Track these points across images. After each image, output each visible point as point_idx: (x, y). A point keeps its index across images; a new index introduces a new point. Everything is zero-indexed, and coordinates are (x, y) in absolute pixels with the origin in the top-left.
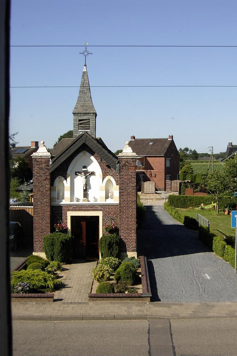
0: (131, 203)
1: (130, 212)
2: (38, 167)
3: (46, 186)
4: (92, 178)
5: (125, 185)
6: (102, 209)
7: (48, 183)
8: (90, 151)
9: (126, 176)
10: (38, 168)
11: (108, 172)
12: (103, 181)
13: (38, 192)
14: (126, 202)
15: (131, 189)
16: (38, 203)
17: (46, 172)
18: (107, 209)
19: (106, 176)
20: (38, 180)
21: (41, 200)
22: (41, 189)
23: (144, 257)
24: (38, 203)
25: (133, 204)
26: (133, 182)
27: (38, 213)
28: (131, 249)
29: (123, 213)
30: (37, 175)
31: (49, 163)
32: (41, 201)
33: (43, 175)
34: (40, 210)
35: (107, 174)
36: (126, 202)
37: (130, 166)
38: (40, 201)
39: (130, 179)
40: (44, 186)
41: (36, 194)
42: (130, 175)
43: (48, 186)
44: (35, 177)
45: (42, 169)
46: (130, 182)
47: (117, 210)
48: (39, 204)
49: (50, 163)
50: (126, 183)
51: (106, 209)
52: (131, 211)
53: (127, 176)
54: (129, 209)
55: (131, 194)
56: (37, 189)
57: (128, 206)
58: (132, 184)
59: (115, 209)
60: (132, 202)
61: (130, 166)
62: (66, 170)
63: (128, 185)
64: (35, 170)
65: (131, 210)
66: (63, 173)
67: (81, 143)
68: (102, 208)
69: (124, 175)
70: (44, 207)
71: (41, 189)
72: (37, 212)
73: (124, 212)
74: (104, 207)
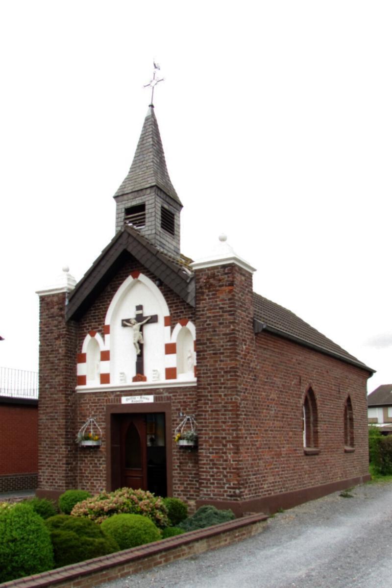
0: (223, 376)
1: (223, 397)
4: (149, 329)
5: (208, 332)
6: (170, 397)
9: (211, 309)
14: (212, 373)
21: (51, 379)
25: (229, 377)
28: (226, 491)
34: (48, 401)
42: (221, 306)
46: (220, 324)
48: (47, 388)
49: (67, 303)
51: (179, 395)
52: (225, 395)
55: (223, 353)
60: (226, 372)
63: (215, 331)
65: (222, 394)
66: (99, 325)
67: (120, 250)
68: (171, 395)
69: (206, 309)
73: (208, 400)
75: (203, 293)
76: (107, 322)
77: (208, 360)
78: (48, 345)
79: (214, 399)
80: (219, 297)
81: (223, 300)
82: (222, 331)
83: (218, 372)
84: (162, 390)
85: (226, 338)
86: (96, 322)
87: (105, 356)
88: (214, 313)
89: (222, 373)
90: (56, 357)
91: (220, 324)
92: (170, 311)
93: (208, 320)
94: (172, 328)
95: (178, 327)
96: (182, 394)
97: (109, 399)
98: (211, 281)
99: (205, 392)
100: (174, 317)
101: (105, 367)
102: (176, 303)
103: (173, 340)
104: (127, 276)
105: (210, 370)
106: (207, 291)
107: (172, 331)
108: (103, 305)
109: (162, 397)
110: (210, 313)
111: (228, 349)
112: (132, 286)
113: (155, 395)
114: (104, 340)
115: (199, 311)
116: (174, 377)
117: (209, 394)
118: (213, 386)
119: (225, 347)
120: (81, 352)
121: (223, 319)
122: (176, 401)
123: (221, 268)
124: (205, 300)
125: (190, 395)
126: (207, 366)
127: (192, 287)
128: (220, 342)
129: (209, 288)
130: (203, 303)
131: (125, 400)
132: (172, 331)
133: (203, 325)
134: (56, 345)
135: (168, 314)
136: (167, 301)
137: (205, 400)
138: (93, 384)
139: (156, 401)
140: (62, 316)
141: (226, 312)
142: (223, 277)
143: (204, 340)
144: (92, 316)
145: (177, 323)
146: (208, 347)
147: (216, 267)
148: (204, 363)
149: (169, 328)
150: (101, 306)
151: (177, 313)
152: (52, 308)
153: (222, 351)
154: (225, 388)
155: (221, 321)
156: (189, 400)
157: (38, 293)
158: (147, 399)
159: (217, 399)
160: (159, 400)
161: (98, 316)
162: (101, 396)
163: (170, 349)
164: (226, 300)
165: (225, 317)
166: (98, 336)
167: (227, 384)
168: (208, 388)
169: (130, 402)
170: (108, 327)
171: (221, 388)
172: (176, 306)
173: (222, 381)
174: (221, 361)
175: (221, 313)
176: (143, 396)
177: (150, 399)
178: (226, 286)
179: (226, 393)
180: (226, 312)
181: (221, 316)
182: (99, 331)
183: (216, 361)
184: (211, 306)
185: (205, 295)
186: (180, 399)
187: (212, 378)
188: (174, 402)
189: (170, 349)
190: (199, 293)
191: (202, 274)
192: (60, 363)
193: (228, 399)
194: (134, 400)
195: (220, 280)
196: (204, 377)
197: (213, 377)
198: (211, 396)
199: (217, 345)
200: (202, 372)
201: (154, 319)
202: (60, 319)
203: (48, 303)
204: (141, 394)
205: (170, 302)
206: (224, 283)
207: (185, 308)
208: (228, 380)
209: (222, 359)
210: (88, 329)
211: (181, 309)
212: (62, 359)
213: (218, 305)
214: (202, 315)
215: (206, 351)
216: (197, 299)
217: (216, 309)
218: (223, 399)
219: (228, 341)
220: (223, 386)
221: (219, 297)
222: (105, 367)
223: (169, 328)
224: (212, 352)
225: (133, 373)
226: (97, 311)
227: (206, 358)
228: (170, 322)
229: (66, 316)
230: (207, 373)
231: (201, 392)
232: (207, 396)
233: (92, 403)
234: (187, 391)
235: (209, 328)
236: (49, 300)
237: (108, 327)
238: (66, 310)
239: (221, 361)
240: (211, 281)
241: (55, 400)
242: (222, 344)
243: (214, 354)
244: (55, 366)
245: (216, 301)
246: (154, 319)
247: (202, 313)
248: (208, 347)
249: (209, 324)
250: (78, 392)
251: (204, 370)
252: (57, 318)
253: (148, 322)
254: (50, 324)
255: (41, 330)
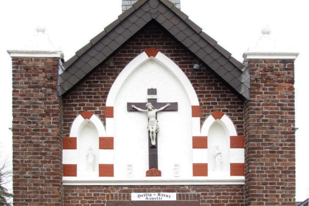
0: (281, 176)
1: (280, 197)
2: (27, 80)
3: (47, 131)
5: (264, 128)
6: (199, 195)
7: (54, 123)
8: (166, 50)
9: (269, 105)
10: (26, 83)
11: (216, 103)
12: (201, 131)
13: (27, 146)
14: (269, 172)
15: (280, 140)
16: (27, 174)
17: (49, 95)
18: (213, 194)
19: (205, 115)
20: (25, 115)
21: (36, 166)
22: (33, 139)
23: (2, 175)
24: (27, 174)
25: (288, 178)
26: (286, 121)
27: (27, 200)
29: (259, 200)
30: (25, 101)
31: (57, 72)
32: (33, 170)
33: (40, 102)
34: (30, 193)
35: (212, 107)
36: (269, 172)
37: (279, 81)
38: (30, 169)
39: (278, 113)
40: (43, 130)
41: (21, 150)
42: (280, 102)
43: (53, 131)
44: (18, 107)
45: (36, 86)
46: (279, 121)
47: (240, 198)
48: (29, 177)
49: (60, 72)
50: (268, 124)
51: (210, 194)
52: (283, 196)
53: (270, 105)
54: (274, 192)
55: (281, 152)
56: (22, 138)
57: (274, 184)
58: (284, 127)
59: (234, 194)
60: (285, 172)
61: (279, 81)
62: (103, 97)
63: (272, 128)
64: (19, 90)
65: (280, 194)
66: (96, 105)
67: (148, 19)
68: (200, 193)
69: (261, 103)
70: (42, 185)
71: (33, 139)
72: (22, 196)
73: (263, 200)
74: (204, 190)
75: (258, 86)
76: (109, 103)
77: (264, 158)
78: (29, 123)
79: (270, 200)
80: (278, 93)
81: (282, 96)
82: (281, 129)
83: (276, 172)
84: (187, 188)
85: (285, 137)
86: (91, 101)
87: (106, 143)
88: (271, 109)
89: (280, 173)
90: (43, 138)
91: (279, 121)
92: (199, 100)
93: (264, 116)
94: (202, 120)
95: (210, 120)
96: (214, 193)
97: (112, 195)
98: (269, 74)
99: (260, 192)
100: (205, 107)
101: (106, 157)
102: (208, 92)
103: (204, 133)
104: (140, 52)
105: (265, 169)
106: (263, 84)
107: (201, 124)
108: (101, 82)
109: (187, 195)
110: (267, 108)
111: (287, 148)
112: (142, 65)
113: (178, 193)
114: (105, 124)
115: (254, 105)
116: (205, 174)
117: (264, 194)
118: (269, 185)
119: (284, 146)
120: (68, 135)
121: (282, 117)
122: (206, 200)
123: (280, 62)
124: (261, 93)
125: (224, 194)
126: (262, 164)
127: (246, 78)
128: (278, 141)
129: (265, 82)
130: (258, 97)
131: (135, 197)
132: (201, 124)
133: (258, 120)
134: (43, 123)
135: (196, 102)
136: (195, 89)
137: (259, 200)
138: (87, 175)
139: (180, 199)
140: (54, 88)
141: (286, 109)
142: (283, 72)
143: (259, 136)
144: (84, 93)
145: (208, 115)
146: (263, 144)
147: (275, 61)
148: (258, 160)
149: (198, 119)
150: (99, 83)
151: (209, 103)
152: (34, 75)
153: (280, 150)
154: (283, 188)
155: (280, 118)
156: (222, 200)
157: (9, 52)
158: (167, 196)
159: (274, 199)
160: (184, 199)
161: (95, 94)
162: (100, 191)
163: (200, 143)
164: (285, 97)
165: (284, 115)
166: (95, 119)
167: (286, 184)
168: (263, 188)
169: (143, 199)
170: (111, 109)
171: (278, 188)
172: (206, 96)
173: (280, 181)
174: (279, 160)
175: (280, 110)
176: (161, 193)
177: (173, 197)
178: (286, 82)
179: (284, 193)
180: (286, 109)
181: (279, 113)
182: (96, 113)
183: (274, 160)
184: (268, 100)
185: (261, 88)
186: (212, 198)
187: (268, 178)
188: (203, 201)
189: (200, 143)
190: (254, 85)
191: (258, 66)
192: (50, 146)
193: (286, 200)
194: (149, 197)
195: (279, 75)
196: (258, 176)
197: (269, 176)
198: (266, 196)
199: (275, 143)
200: (256, 170)
201: (173, 107)
202: (49, 91)
203: (25, 69)
204: (158, 191)
205: (198, 90)
206: (284, 79)
207: (218, 100)
208: (287, 181)
209: (280, 158)
210: (80, 109)
211: (214, 100)
212: (53, 142)
213: (276, 101)
214: (257, 109)
215: (262, 148)
216: (253, 93)
217: (274, 105)
218: (281, 200)
219: (287, 141)
220: (281, 186)
221: (278, 93)
222: (106, 157)
223: (198, 119)
224: (268, 150)
225: (146, 167)
226: (93, 88)
227: (262, 156)
228: (199, 112)
229: (59, 89)
230: (263, 172)
231: (255, 192)
232: (262, 196)
233: (86, 198)
234: (221, 190)
235: (265, 124)
236: (30, 64)
237: (111, 109)
238: (60, 81)
239: (279, 160)
240: (269, 74)
241: (42, 193)
242: (280, 142)
243: (270, 152)
244: (42, 149)
245: (274, 97)
246: (173, 107)
247: (256, 107)
248: (263, 144)
249: (266, 121)
250: (64, 184)
251: (258, 168)
252: (43, 88)
253: (164, 110)
254: (32, 95)
255: (16, 103)
